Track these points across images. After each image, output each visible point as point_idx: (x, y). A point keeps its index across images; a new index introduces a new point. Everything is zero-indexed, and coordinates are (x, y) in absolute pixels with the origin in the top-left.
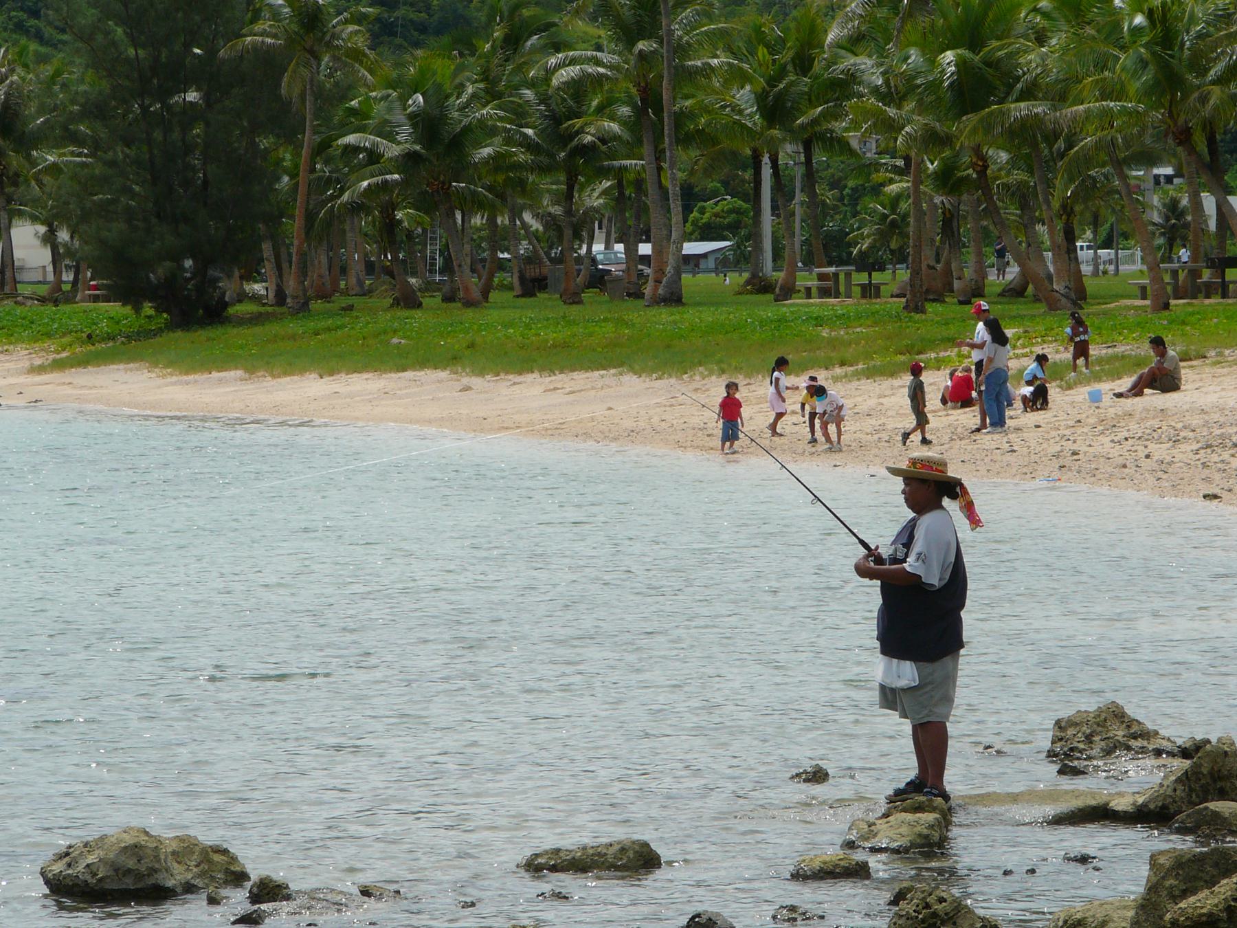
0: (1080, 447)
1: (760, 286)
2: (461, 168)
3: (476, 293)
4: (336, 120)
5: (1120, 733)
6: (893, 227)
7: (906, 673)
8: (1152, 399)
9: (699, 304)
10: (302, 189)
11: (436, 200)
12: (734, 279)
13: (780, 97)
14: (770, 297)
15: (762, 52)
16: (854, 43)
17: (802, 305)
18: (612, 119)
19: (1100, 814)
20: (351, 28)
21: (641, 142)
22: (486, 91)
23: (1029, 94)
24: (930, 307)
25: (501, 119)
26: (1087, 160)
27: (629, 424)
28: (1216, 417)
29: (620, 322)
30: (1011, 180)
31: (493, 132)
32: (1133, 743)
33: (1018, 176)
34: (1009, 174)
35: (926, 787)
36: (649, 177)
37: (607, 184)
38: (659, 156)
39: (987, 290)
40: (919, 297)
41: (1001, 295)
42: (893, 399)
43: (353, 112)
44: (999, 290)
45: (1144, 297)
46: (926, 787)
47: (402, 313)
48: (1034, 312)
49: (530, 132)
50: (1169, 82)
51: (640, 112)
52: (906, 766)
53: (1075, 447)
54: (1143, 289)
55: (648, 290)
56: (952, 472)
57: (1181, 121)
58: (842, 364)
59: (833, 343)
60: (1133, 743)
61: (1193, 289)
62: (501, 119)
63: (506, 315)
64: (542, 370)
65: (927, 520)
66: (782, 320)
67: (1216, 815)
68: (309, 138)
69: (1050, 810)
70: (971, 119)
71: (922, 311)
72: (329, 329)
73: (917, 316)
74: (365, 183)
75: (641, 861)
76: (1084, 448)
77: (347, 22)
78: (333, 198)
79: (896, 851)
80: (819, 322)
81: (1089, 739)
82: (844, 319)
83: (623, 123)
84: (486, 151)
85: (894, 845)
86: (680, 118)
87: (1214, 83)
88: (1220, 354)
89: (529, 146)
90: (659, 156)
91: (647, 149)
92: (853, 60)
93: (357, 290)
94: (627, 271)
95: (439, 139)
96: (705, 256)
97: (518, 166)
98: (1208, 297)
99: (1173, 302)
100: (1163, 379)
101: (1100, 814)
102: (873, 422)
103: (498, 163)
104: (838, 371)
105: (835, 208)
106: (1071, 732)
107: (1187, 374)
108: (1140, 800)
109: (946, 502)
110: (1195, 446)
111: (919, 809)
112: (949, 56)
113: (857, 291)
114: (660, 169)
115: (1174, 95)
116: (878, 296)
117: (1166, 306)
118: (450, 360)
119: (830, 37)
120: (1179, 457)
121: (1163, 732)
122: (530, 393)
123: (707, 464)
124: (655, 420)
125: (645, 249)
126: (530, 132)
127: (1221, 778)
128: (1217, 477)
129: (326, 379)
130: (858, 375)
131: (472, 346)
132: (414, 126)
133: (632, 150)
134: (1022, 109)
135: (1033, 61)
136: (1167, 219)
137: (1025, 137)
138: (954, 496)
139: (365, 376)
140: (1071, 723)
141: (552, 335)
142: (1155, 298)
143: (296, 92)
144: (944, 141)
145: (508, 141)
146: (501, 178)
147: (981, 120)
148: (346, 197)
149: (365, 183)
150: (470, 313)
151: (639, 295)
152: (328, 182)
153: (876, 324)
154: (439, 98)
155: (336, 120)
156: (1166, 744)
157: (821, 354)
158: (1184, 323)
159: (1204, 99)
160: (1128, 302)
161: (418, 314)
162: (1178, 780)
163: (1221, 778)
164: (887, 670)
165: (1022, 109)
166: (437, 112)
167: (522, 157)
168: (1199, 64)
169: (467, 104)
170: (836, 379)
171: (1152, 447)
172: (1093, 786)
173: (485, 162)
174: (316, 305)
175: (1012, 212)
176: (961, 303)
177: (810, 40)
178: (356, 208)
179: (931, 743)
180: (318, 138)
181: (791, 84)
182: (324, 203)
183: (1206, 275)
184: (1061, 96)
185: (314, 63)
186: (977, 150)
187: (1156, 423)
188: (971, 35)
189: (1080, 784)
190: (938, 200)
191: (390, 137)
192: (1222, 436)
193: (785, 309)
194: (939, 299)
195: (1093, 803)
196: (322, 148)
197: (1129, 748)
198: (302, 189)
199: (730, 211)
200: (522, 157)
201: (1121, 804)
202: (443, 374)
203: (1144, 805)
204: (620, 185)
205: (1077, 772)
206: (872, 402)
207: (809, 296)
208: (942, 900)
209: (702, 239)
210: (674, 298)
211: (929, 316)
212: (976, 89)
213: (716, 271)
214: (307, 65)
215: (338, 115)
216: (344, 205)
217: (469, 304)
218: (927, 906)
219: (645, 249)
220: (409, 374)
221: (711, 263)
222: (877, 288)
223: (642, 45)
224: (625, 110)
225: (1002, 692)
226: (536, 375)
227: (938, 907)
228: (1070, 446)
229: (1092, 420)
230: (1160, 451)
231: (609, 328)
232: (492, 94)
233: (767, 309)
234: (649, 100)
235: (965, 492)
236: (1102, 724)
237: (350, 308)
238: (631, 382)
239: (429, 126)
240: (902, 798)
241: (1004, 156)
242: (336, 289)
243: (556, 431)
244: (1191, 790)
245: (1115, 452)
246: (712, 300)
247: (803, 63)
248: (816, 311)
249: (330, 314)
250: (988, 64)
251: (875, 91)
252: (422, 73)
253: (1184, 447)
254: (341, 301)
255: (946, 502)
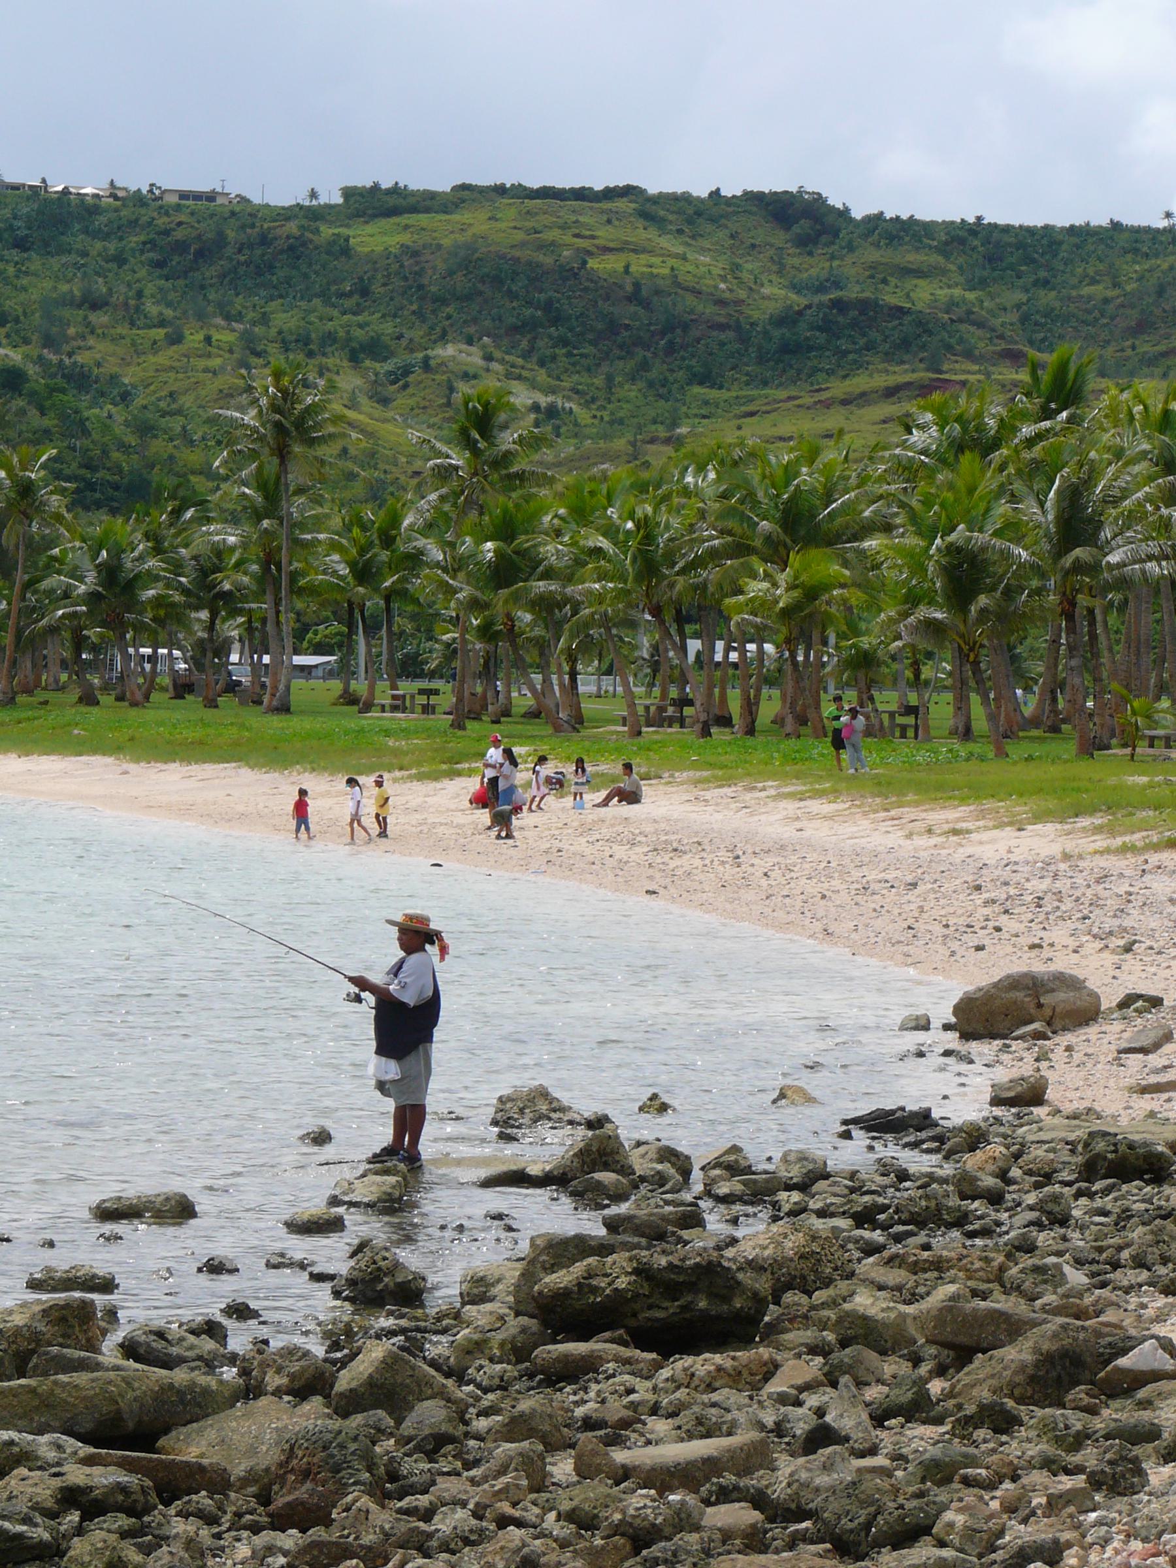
0: (564, 845)
1: (349, 699)
2: (132, 604)
3: (139, 696)
4: (41, 564)
5: (544, 1108)
6: (451, 652)
7: (392, 1070)
8: (618, 809)
9: (302, 713)
10: (13, 614)
11: (116, 623)
12: (336, 686)
13: (368, 564)
14: (356, 708)
15: (356, 531)
16: (429, 528)
17: (378, 718)
18: (245, 573)
19: (518, 1178)
20: (54, 497)
21: (264, 592)
22: (153, 548)
23: (547, 575)
24: (470, 725)
25: (164, 570)
26: (587, 625)
27: (240, 808)
28: (663, 826)
29: (242, 726)
30: (532, 634)
31: (157, 578)
32: (553, 1115)
33: (538, 631)
34: (532, 630)
35: (402, 1154)
36: (271, 615)
37: (241, 620)
38: (277, 603)
39: (514, 710)
40: (466, 713)
41: (524, 716)
42: (435, 799)
43: (54, 559)
44: (523, 710)
45: (624, 725)
46: (402, 1154)
47: (83, 709)
48: (543, 733)
49: (183, 579)
50: (649, 567)
51: (266, 568)
52: (384, 1135)
53: (560, 845)
54: (624, 719)
55: (266, 699)
56: (433, 926)
57: (655, 601)
58: (401, 769)
59: (396, 752)
60: (553, 1115)
61: (659, 720)
62: (164, 570)
63: (163, 714)
64: (182, 760)
65: (415, 957)
66: (361, 731)
67: (599, 1182)
68: (21, 577)
69: (483, 1173)
70: (504, 592)
71: (463, 728)
72: (28, 719)
73: (460, 733)
74: (60, 612)
75: (181, 1210)
76: (567, 847)
77: (52, 493)
78: (37, 621)
79: (368, 1205)
80: (387, 733)
81: (521, 1111)
82: (406, 733)
83: (253, 576)
84: (152, 592)
85: (366, 1200)
86: (294, 576)
87: (678, 573)
88: (672, 776)
89: (185, 591)
90: (277, 603)
91: (269, 597)
92: (424, 541)
93: (54, 686)
94: (253, 683)
95: (117, 586)
96: (316, 666)
97: (173, 605)
98: (670, 726)
99: (644, 729)
100: (631, 797)
101: (518, 1178)
102: (418, 816)
103: (158, 602)
104: (398, 774)
105: (412, 635)
106: (509, 1105)
107: (646, 789)
108: (548, 1168)
109: (428, 947)
110: (646, 849)
111: (386, 1172)
112: (489, 545)
113: (419, 709)
114: (278, 612)
115: (650, 582)
116: (433, 713)
117: (639, 733)
118: (115, 749)
119: (406, 523)
120: (634, 857)
121: (575, 1107)
122: (172, 780)
123: (280, 842)
124: (261, 806)
125: (266, 659)
126: (183, 579)
127: (605, 1154)
128: (658, 875)
129: (23, 759)
130: (411, 778)
131: (132, 739)
132: (99, 572)
133: (259, 596)
134: (541, 586)
135: (552, 551)
136: (652, 656)
137: (545, 607)
138: (432, 943)
139: (52, 758)
140: (510, 1099)
141: (192, 734)
142: (632, 727)
143: (13, 542)
144: (486, 606)
145: (168, 586)
146: (162, 612)
147: (511, 594)
148: (44, 622)
149: (60, 612)
150: (133, 712)
151: (258, 702)
152: (34, 609)
153: (429, 737)
154: (117, 552)
155: (41, 564)
156: (578, 1118)
157: (386, 760)
158: (649, 750)
159: (672, 586)
160: (613, 728)
161: (95, 710)
162: (575, 1155)
163: (605, 1154)
164: (377, 1067)
165: (541, 586)
166: (115, 562)
167: (178, 598)
168: (670, 558)
169: (137, 556)
170: (395, 780)
171: (615, 847)
172: (514, 1155)
173: (150, 601)
174: (21, 699)
175: (531, 656)
176: (493, 722)
177: (395, 520)
178: (53, 630)
179: (410, 1119)
180: (26, 577)
181: (375, 555)
182: (29, 625)
183: (671, 710)
184: (569, 579)
185: (27, 522)
186: (509, 616)
187: (620, 829)
188: (506, 531)
189: (509, 1150)
190: (478, 646)
191: (81, 579)
192: (666, 842)
193: (364, 722)
194: (477, 718)
195: (514, 1168)
196: (29, 585)
197: (550, 1119)
198: (13, 614)
199: (337, 634)
200: (178, 598)
201: (534, 1170)
202: (110, 760)
203: (550, 1172)
204: (250, 621)
205: (510, 1139)
206: (420, 800)
207: (383, 711)
208: (385, 1259)
209: (315, 654)
210: (284, 708)
211: (468, 733)
212: (504, 573)
213: (324, 678)
214: (21, 523)
215: (42, 561)
216: (44, 627)
217: (135, 704)
218: (375, 1263)
219: (266, 659)
220: (84, 758)
221: (320, 672)
222: (434, 707)
223: (266, 523)
224: (255, 567)
225: (463, 1075)
226: (177, 765)
227: (382, 1263)
228: (557, 844)
229: (575, 824)
230: (620, 851)
231: (234, 730)
232: (158, 550)
233: (351, 720)
234: (270, 560)
235: (441, 939)
236: (532, 1100)
237: (46, 703)
238: (246, 775)
239: (110, 574)
240: (382, 1159)
241: (528, 617)
242: (37, 685)
243: (185, 811)
244: (584, 1163)
245: (588, 851)
246: (313, 712)
247: (388, 540)
248: (386, 724)
249: (31, 707)
250: (517, 553)
251: (437, 565)
252: (106, 533)
253: (637, 849)
254: (41, 696)
255: (428, 947)
